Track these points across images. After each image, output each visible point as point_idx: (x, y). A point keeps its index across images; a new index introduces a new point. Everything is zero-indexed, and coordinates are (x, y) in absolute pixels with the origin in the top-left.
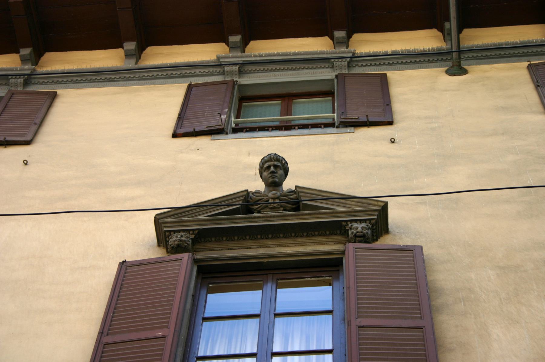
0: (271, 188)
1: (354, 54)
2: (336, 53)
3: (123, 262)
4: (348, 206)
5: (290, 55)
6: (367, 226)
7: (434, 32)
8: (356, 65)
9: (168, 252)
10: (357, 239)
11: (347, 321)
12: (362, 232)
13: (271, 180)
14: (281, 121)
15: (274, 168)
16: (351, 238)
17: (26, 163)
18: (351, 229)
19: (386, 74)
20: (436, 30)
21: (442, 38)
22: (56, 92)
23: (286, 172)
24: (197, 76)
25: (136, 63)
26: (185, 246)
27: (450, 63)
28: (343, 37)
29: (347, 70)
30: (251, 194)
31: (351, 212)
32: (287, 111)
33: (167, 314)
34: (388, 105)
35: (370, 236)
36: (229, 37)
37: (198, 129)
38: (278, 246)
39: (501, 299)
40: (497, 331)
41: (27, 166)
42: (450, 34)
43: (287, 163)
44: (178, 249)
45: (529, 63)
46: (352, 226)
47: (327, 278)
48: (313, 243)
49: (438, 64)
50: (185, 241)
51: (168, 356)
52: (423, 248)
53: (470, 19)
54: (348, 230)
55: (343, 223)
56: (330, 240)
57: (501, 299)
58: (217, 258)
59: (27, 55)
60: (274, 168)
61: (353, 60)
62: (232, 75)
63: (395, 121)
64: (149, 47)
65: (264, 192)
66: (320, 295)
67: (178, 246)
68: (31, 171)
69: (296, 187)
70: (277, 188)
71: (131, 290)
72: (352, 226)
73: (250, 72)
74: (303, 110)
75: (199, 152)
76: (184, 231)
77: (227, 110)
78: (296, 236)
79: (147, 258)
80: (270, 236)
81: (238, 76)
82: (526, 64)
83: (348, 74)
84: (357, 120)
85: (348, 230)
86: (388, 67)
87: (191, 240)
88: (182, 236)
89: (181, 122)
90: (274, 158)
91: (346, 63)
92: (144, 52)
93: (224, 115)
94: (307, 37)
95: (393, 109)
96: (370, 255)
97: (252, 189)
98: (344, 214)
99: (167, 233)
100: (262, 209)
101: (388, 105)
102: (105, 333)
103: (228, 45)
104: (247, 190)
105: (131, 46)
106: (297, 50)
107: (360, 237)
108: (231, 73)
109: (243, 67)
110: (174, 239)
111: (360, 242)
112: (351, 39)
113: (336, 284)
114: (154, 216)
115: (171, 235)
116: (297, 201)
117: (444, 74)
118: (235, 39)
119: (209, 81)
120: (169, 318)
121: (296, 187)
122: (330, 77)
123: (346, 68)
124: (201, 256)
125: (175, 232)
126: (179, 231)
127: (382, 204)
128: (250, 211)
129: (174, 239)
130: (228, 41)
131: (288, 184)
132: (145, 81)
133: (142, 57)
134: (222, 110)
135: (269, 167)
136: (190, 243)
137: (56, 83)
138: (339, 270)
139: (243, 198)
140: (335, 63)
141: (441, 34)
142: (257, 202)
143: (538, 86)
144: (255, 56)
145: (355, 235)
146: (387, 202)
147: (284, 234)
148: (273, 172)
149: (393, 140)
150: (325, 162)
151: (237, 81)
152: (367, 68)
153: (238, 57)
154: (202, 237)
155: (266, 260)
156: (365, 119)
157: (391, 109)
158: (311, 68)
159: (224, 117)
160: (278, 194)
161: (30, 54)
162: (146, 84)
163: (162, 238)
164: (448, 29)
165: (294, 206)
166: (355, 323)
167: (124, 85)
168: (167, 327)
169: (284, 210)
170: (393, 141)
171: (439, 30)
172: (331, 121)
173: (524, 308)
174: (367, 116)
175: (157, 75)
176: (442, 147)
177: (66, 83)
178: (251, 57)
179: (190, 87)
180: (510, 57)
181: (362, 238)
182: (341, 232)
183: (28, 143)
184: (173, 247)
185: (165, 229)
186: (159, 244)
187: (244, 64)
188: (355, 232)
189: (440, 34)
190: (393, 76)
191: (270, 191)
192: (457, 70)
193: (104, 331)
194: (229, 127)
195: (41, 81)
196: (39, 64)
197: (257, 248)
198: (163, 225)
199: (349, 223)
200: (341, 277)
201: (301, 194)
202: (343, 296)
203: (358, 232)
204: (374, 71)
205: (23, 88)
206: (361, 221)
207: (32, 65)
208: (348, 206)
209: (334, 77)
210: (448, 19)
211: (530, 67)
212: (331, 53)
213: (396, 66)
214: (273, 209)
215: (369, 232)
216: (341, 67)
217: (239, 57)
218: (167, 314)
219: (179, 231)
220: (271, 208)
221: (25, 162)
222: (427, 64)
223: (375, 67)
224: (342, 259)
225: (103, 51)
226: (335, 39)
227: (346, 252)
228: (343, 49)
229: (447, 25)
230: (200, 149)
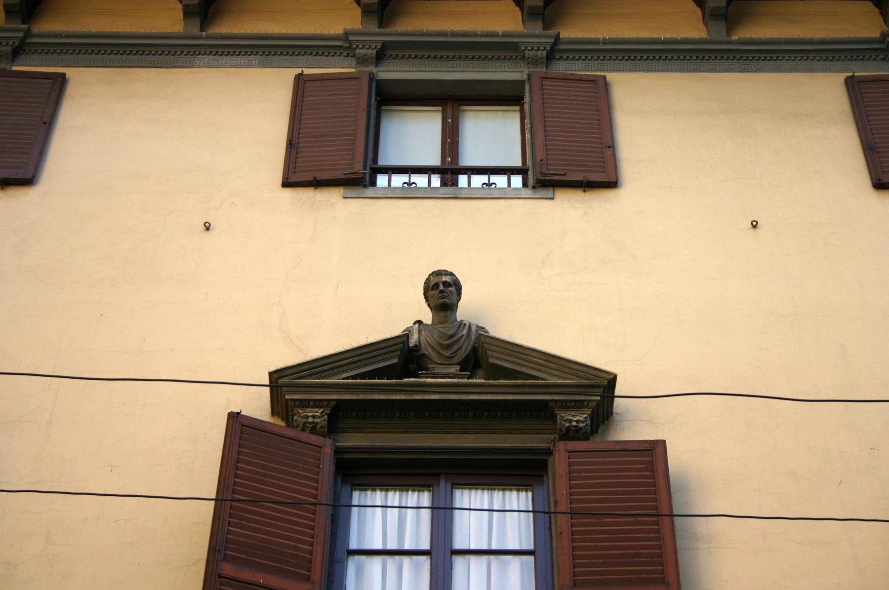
20: (871, 4)
22: (64, 74)
51: (363, 151)
123: (374, 60)
135: (437, 285)
138: (542, 476)
140: (527, 52)
148: (442, 292)
154: (341, 415)
179: (299, 78)
185: (287, 397)
198: (284, 389)
200: (545, 479)
201: (489, 353)
202: (543, 515)
209: (525, 77)
211: (852, 84)
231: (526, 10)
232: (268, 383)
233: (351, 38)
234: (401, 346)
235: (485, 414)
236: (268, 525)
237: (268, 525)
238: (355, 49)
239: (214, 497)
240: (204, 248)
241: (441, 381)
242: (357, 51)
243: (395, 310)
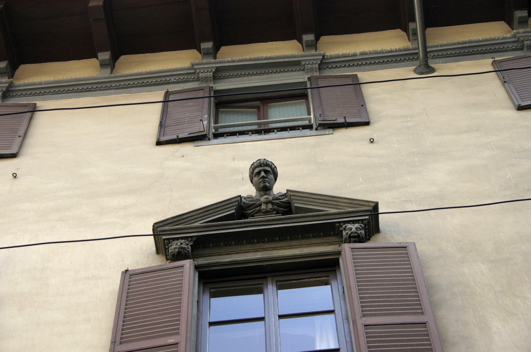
0: (262, 193)
1: (324, 56)
2: (306, 56)
3: (126, 271)
4: (339, 207)
5: (262, 60)
6: (361, 226)
7: (399, 32)
8: (327, 67)
9: (167, 260)
10: (352, 239)
11: (349, 320)
13: (262, 185)
14: (259, 124)
15: (264, 173)
16: (346, 239)
17: (15, 176)
18: (345, 229)
19: (356, 75)
21: (407, 37)
24: (173, 83)
25: (111, 73)
26: (186, 253)
27: (417, 63)
28: (312, 41)
29: (318, 73)
30: (243, 200)
31: (343, 213)
32: (261, 114)
34: (362, 105)
35: (364, 236)
36: (201, 44)
37: (181, 136)
38: (274, 249)
39: (495, 292)
40: (496, 324)
41: (16, 180)
42: (415, 34)
43: (276, 167)
44: (179, 256)
45: (493, 60)
46: (346, 227)
47: (324, 278)
48: (309, 245)
49: (405, 63)
50: (184, 248)
52: (417, 245)
53: (435, 18)
54: (342, 231)
55: (337, 225)
56: (324, 241)
57: (495, 292)
58: (217, 263)
59: (4, 68)
60: (264, 173)
61: (324, 63)
62: (207, 81)
63: (371, 121)
64: (22, 65)
65: (256, 196)
66: (318, 296)
67: (179, 253)
68: (22, 183)
69: (287, 190)
70: (268, 192)
71: (137, 299)
72: (346, 227)
73: (224, 78)
74: (279, 114)
75: (185, 158)
76: (182, 238)
77: (207, 116)
78: (291, 239)
79: (147, 266)
80: (266, 240)
81: (212, 82)
82: (491, 60)
83: (320, 76)
84: (335, 122)
85: (342, 231)
86: (357, 68)
87: (190, 247)
88: (181, 244)
89: (162, 130)
90: (263, 163)
91: (317, 65)
92: (118, 61)
93: (205, 121)
94: (276, 41)
95: (368, 109)
97: (244, 195)
98: (337, 216)
99: (166, 241)
100: (256, 213)
101: (362, 105)
102: (118, 342)
103: (200, 52)
104: (240, 196)
105: (105, 56)
106: (269, 55)
107: (354, 237)
108: (206, 79)
109: (219, 74)
110: (174, 247)
111: (355, 242)
113: (334, 283)
114: (152, 224)
115: (170, 243)
116: (286, 205)
117: (413, 73)
118: (208, 45)
119: (185, 88)
120: (179, 325)
121: (287, 190)
122: (302, 80)
123: (318, 70)
124: (201, 261)
125: (174, 239)
126: (178, 239)
127: (373, 205)
128: (245, 216)
129: (174, 247)
130: (200, 48)
131: (279, 188)
132: (122, 90)
133: (116, 66)
134: (202, 116)
135: (259, 173)
136: (190, 250)
137: (34, 95)
138: (335, 270)
139: (235, 207)
140: (306, 66)
141: (405, 34)
142: (249, 206)
143: (505, 82)
144: (229, 62)
145: (350, 235)
146: (378, 203)
147: (280, 238)
148: (263, 177)
149: (372, 140)
150: (311, 165)
151: (212, 87)
152: (337, 69)
153: (211, 64)
154: (201, 245)
155: (265, 264)
156: (343, 121)
157: (366, 109)
158: (286, 72)
159: (205, 123)
160: (271, 198)
161: (6, 68)
162: (123, 93)
163: (162, 247)
164: (413, 29)
165: (286, 210)
166: (362, 321)
167: (101, 95)
168: (178, 334)
169: (277, 213)
170: (372, 141)
172: (306, 123)
173: (519, 300)
174: (345, 117)
175: (134, 83)
176: (420, 145)
177: (43, 94)
178: (224, 62)
180: (474, 54)
181: (358, 239)
182: (334, 233)
183: (14, 156)
184: (173, 255)
185: (164, 237)
186: (158, 252)
187: (218, 70)
188: (349, 232)
189: (404, 34)
190: (364, 76)
191: (262, 196)
192: (426, 70)
193: (117, 340)
194: (211, 133)
195: (19, 93)
196: (15, 77)
197: (255, 251)
199: (342, 224)
200: (338, 277)
203: (352, 233)
204: (344, 72)
205: (2, 102)
206: (354, 222)
207: (9, 78)
208: (339, 207)
209: (306, 80)
210: (413, 20)
213: (365, 67)
214: (267, 212)
215: (363, 232)
216: (312, 70)
217: (213, 64)
219: (178, 239)
220: (264, 212)
221: (15, 175)
222: (395, 64)
223: (345, 69)
224: (337, 260)
225: (78, 61)
226: (304, 42)
227: (343, 253)
228: (313, 52)
229: (411, 26)
230: (185, 156)
231: (304, 45)
232: (152, 233)
233: (195, 67)
234: (236, 203)
236: (159, 291)
237: (159, 291)
238: (198, 73)
239: (162, 100)
240: (110, 168)
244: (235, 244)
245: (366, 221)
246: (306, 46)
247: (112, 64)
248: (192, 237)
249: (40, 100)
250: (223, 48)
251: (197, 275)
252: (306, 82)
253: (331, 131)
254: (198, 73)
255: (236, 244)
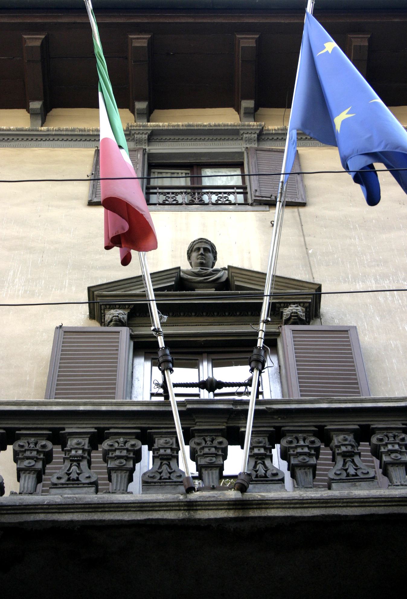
12: (118, 316)
23: (215, 253)
33: (63, 376)
91: (256, 135)
94: (18, 108)
96: (85, 338)
109: (154, 136)
112: (152, 115)
123: (147, 141)
127: (317, 287)
130: (134, 106)
131: (221, 263)
135: (199, 249)
139: (174, 279)
140: (136, 136)
148: (202, 254)
150: (243, 240)
171: (236, 111)
205: (258, 145)
212: (29, 130)
216: (249, 140)
218: (63, 376)
232: (87, 301)
235: (238, 314)
238: (242, 134)
241: (205, 295)
242: (245, 136)
243: (217, 370)
244: (195, 316)
245: (308, 304)
246: (245, 113)
247: (43, 115)
248: (304, 303)
249: (303, 146)
250: (260, 109)
251: (132, 344)
252: (243, 153)
253: (267, 208)
254: (133, 134)
255: (184, 316)
